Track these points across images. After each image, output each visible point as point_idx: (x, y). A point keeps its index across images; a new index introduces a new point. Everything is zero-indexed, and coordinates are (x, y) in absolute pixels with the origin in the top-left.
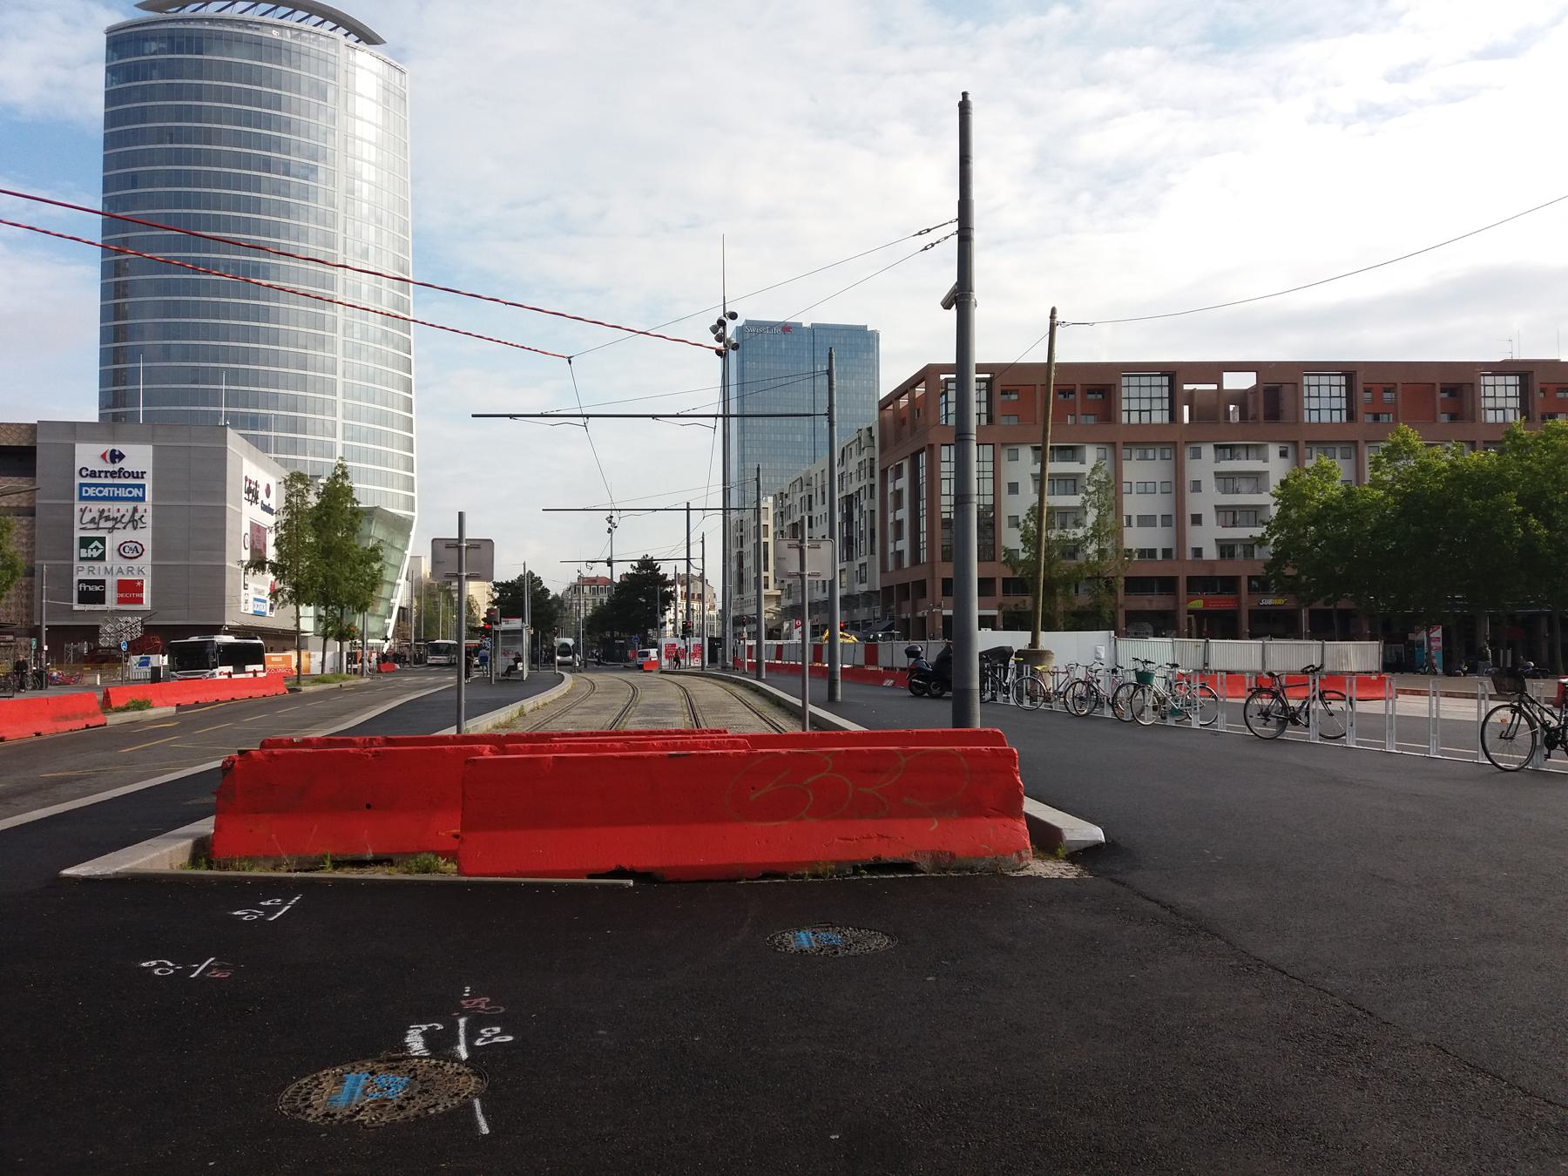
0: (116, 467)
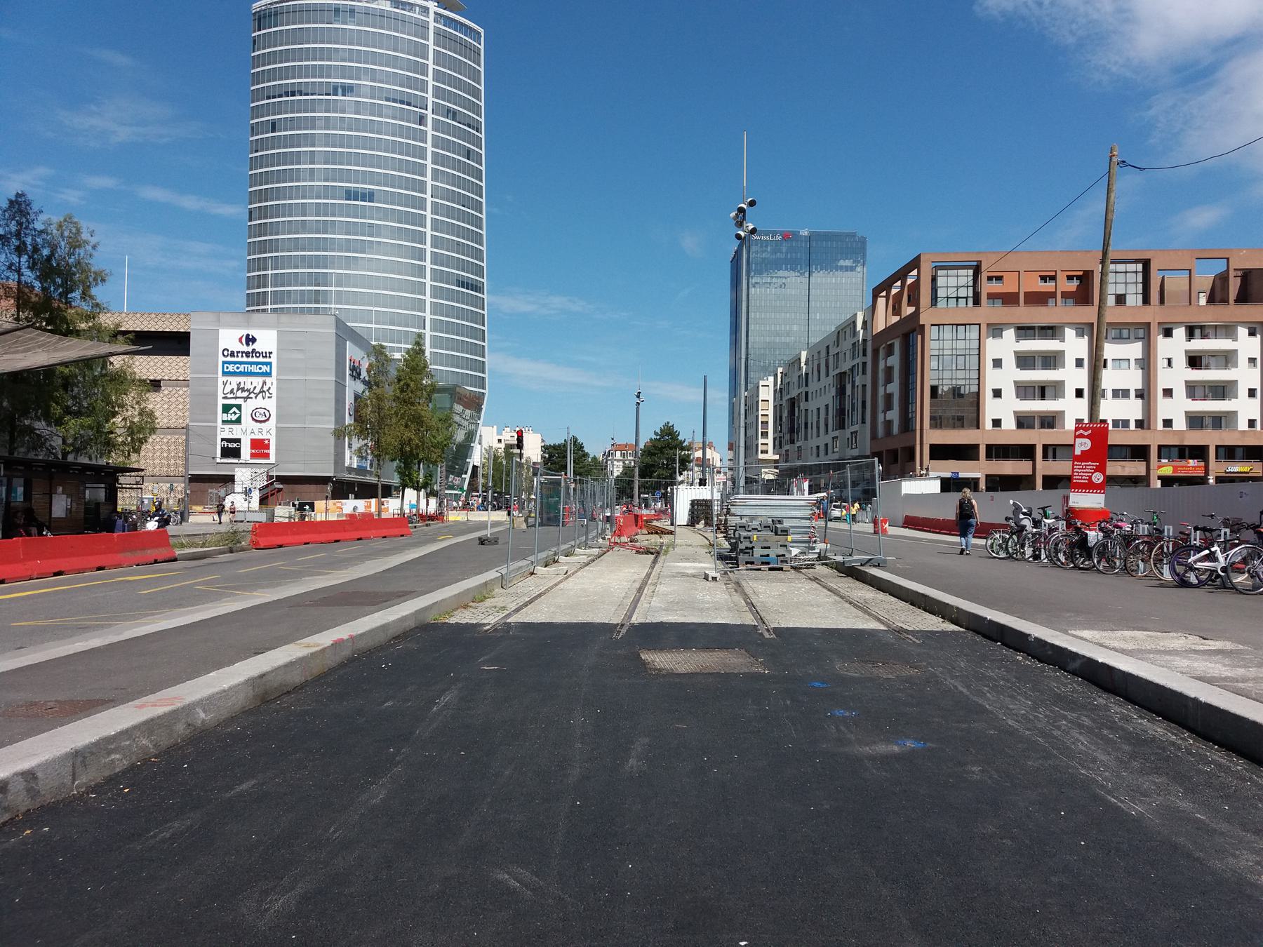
0: (250, 349)
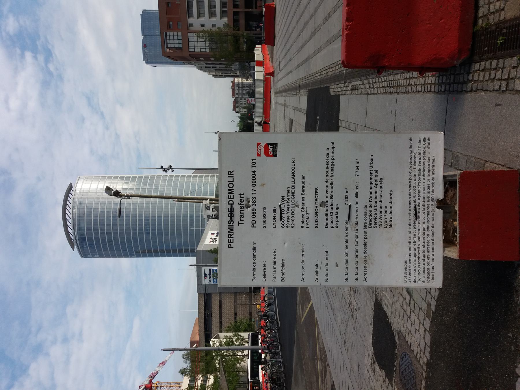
0: (208, 276)
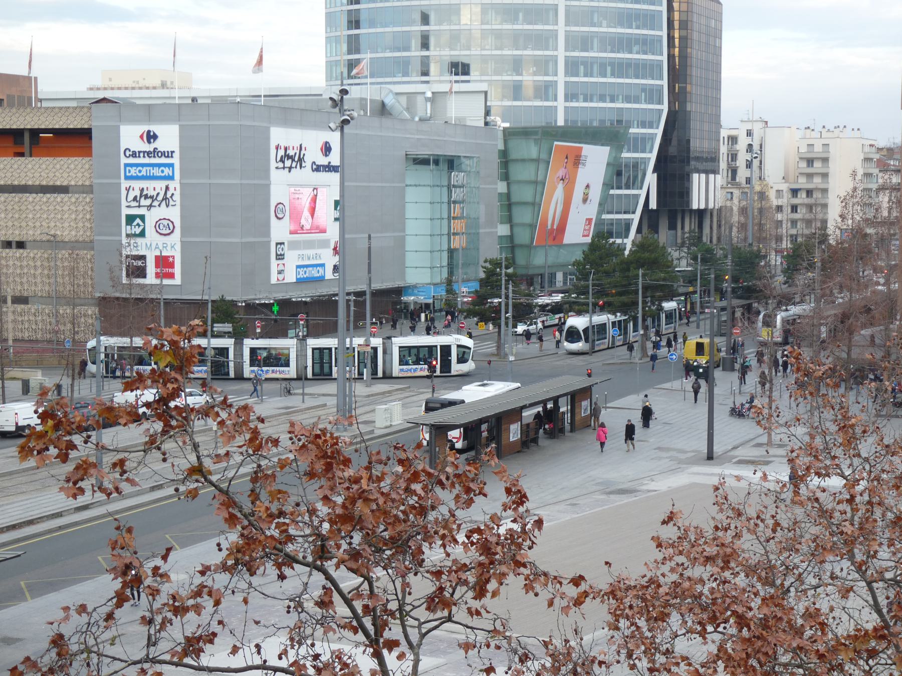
0: (149, 148)
